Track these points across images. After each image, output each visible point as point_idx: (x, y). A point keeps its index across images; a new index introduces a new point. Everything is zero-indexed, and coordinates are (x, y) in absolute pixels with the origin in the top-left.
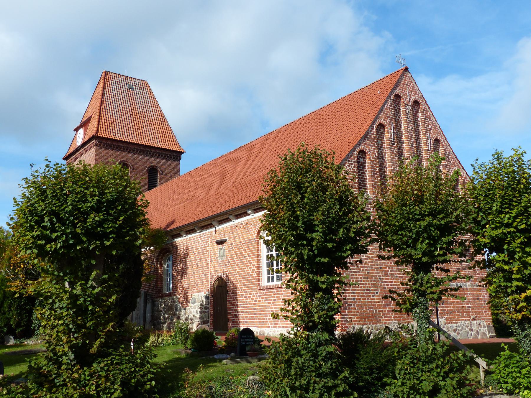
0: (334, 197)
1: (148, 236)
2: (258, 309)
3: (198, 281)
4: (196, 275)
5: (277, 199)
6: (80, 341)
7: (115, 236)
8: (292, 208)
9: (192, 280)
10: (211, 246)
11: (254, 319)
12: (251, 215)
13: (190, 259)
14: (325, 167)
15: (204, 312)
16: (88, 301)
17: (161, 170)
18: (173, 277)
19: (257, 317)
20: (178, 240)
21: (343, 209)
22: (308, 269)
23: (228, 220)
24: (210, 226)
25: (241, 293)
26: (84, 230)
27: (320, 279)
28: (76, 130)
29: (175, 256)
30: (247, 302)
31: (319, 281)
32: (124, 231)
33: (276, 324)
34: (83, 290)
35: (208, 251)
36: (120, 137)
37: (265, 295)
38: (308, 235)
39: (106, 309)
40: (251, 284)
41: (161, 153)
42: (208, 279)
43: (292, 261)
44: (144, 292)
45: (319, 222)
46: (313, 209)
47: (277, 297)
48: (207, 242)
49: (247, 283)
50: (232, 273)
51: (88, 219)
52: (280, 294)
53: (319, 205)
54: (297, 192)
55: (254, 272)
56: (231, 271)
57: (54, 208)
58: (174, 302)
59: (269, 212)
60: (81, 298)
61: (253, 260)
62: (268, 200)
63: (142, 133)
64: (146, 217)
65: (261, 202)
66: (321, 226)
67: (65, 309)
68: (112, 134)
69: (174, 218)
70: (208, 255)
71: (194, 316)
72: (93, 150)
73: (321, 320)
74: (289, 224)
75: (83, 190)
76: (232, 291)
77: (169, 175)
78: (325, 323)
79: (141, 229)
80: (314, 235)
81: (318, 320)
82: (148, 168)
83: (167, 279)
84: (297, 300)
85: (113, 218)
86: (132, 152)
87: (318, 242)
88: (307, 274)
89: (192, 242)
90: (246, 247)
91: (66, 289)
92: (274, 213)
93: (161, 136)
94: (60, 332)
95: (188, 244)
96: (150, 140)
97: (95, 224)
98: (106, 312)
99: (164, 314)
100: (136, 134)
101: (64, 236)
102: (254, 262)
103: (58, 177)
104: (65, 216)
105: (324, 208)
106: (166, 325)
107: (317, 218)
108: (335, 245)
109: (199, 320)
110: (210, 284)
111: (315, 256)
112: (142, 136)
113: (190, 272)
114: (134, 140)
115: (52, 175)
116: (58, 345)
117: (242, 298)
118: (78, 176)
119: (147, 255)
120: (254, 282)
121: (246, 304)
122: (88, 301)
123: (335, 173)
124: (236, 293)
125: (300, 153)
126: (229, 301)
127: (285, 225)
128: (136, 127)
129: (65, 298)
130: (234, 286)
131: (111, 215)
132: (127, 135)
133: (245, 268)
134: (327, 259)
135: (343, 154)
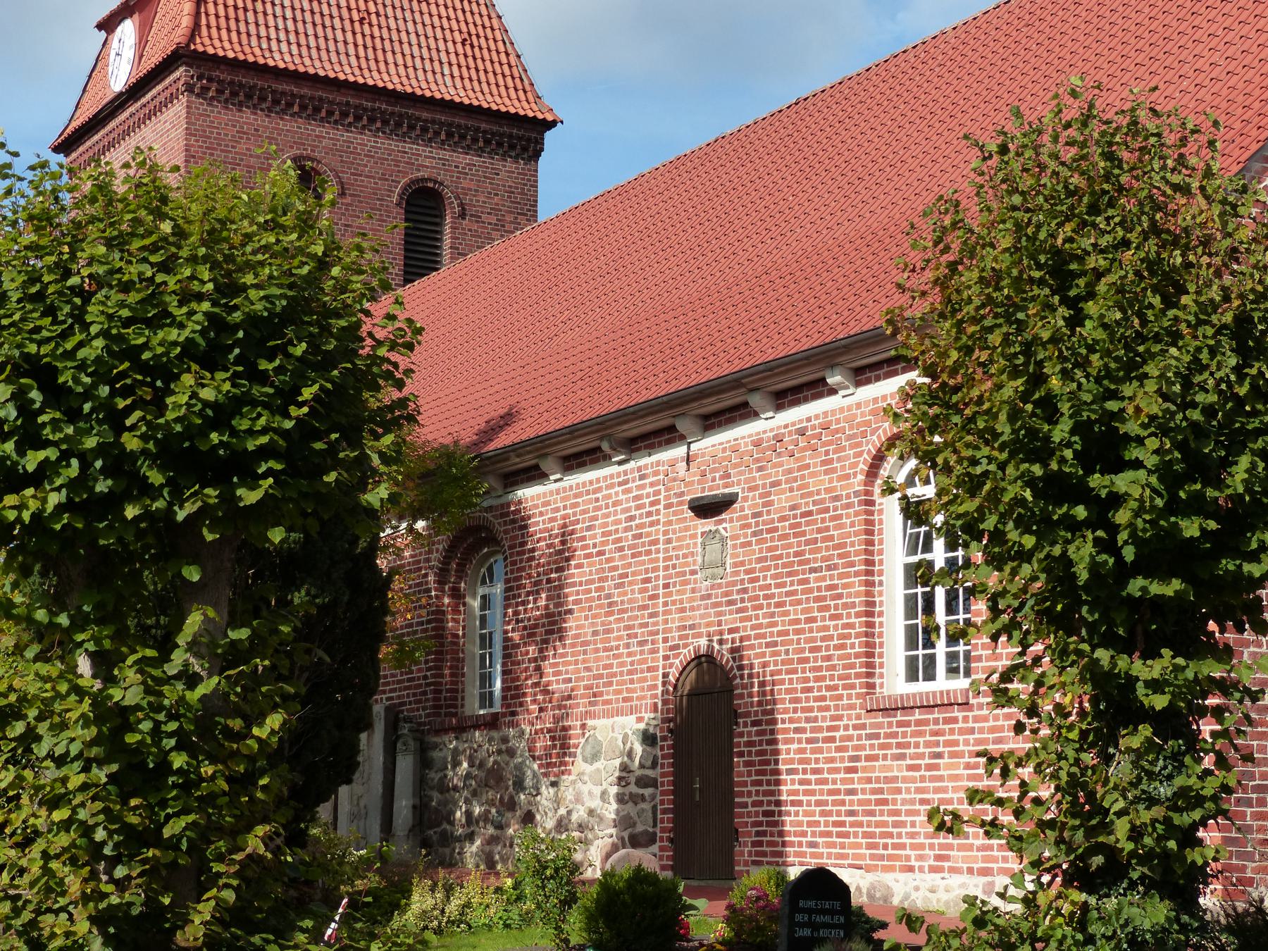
0: (1214, 318)
1: (407, 476)
2: (864, 791)
3: (611, 666)
4: (602, 641)
5: (961, 322)
6: (135, 898)
7: (279, 467)
8: (1026, 364)
9: (584, 661)
10: (669, 523)
11: (846, 835)
12: (842, 393)
13: (580, 575)
14: (1176, 187)
15: (635, 799)
16: (170, 735)
17: (457, 198)
18: (505, 648)
19: (860, 824)
20: (528, 494)
21: (1254, 371)
22: (1092, 627)
23: (741, 412)
24: (667, 436)
25: (791, 721)
26: (156, 439)
27: (1144, 670)
28: (108, 25)
29: (514, 563)
30: (817, 761)
31: (1137, 679)
32: (319, 446)
33: (939, 858)
34: (152, 688)
35: (656, 542)
36: (288, 58)
37: (895, 735)
38: (1095, 480)
39: (242, 769)
40: (835, 688)
41: (459, 126)
42: (653, 660)
43: (1024, 590)
44: (387, 709)
45: (1144, 426)
46: (1118, 370)
47: (948, 743)
48: (653, 504)
49: (817, 679)
50: (757, 637)
51: (173, 393)
52: (962, 732)
53: (1148, 351)
54: (1054, 293)
55: (848, 636)
56: (753, 627)
57: (33, 348)
58: (511, 753)
59: (927, 380)
60: (140, 721)
61: (845, 586)
62: (922, 328)
63: (378, 41)
64: (406, 391)
65: (894, 334)
66: (1152, 443)
67: (77, 766)
68: (254, 42)
69: (512, 401)
70: (657, 560)
71: (591, 812)
72: (177, 110)
73: (1143, 846)
74: (1014, 432)
75: (149, 274)
76: (756, 713)
77: (493, 220)
78: (1158, 856)
79: (388, 439)
80: (1123, 482)
81: (1130, 846)
82: (404, 189)
83: (483, 657)
84: (1043, 755)
85: (271, 391)
86: (336, 122)
87: (1137, 514)
88: (1085, 647)
89: (590, 502)
90: (819, 531)
91: (80, 682)
92: (952, 382)
93: (460, 50)
94: (57, 856)
95: (569, 511)
96: (411, 70)
97: (201, 414)
98: (242, 783)
99: (467, 801)
100: (356, 45)
101: (75, 462)
102: (849, 595)
103: (49, 220)
104: (76, 380)
105: (1168, 367)
106: (474, 848)
107: (1138, 410)
108: (1212, 525)
109: (613, 831)
110: (664, 684)
111: (1124, 572)
112: (380, 53)
113: (578, 627)
114: (348, 70)
115: (24, 209)
116: (49, 910)
117: (796, 746)
118: (129, 216)
119: (398, 553)
120: (848, 677)
121: (815, 771)
122: (170, 735)
123: (1222, 215)
124: (774, 722)
125: (1068, 126)
126: (741, 754)
127: (996, 435)
128: (355, 13)
129: (73, 715)
130: (764, 694)
131: (263, 378)
132: (318, 49)
133: (814, 620)
134: (1176, 585)
135: (1254, 133)
